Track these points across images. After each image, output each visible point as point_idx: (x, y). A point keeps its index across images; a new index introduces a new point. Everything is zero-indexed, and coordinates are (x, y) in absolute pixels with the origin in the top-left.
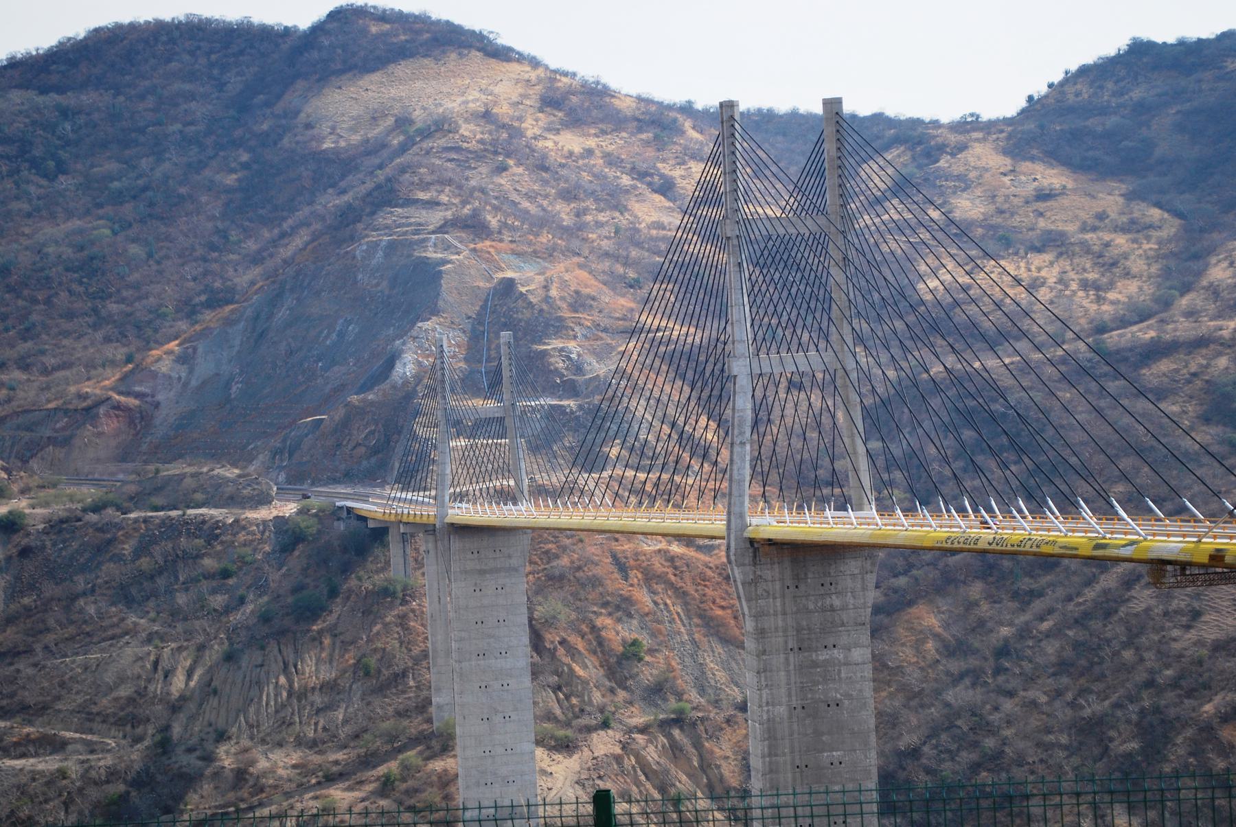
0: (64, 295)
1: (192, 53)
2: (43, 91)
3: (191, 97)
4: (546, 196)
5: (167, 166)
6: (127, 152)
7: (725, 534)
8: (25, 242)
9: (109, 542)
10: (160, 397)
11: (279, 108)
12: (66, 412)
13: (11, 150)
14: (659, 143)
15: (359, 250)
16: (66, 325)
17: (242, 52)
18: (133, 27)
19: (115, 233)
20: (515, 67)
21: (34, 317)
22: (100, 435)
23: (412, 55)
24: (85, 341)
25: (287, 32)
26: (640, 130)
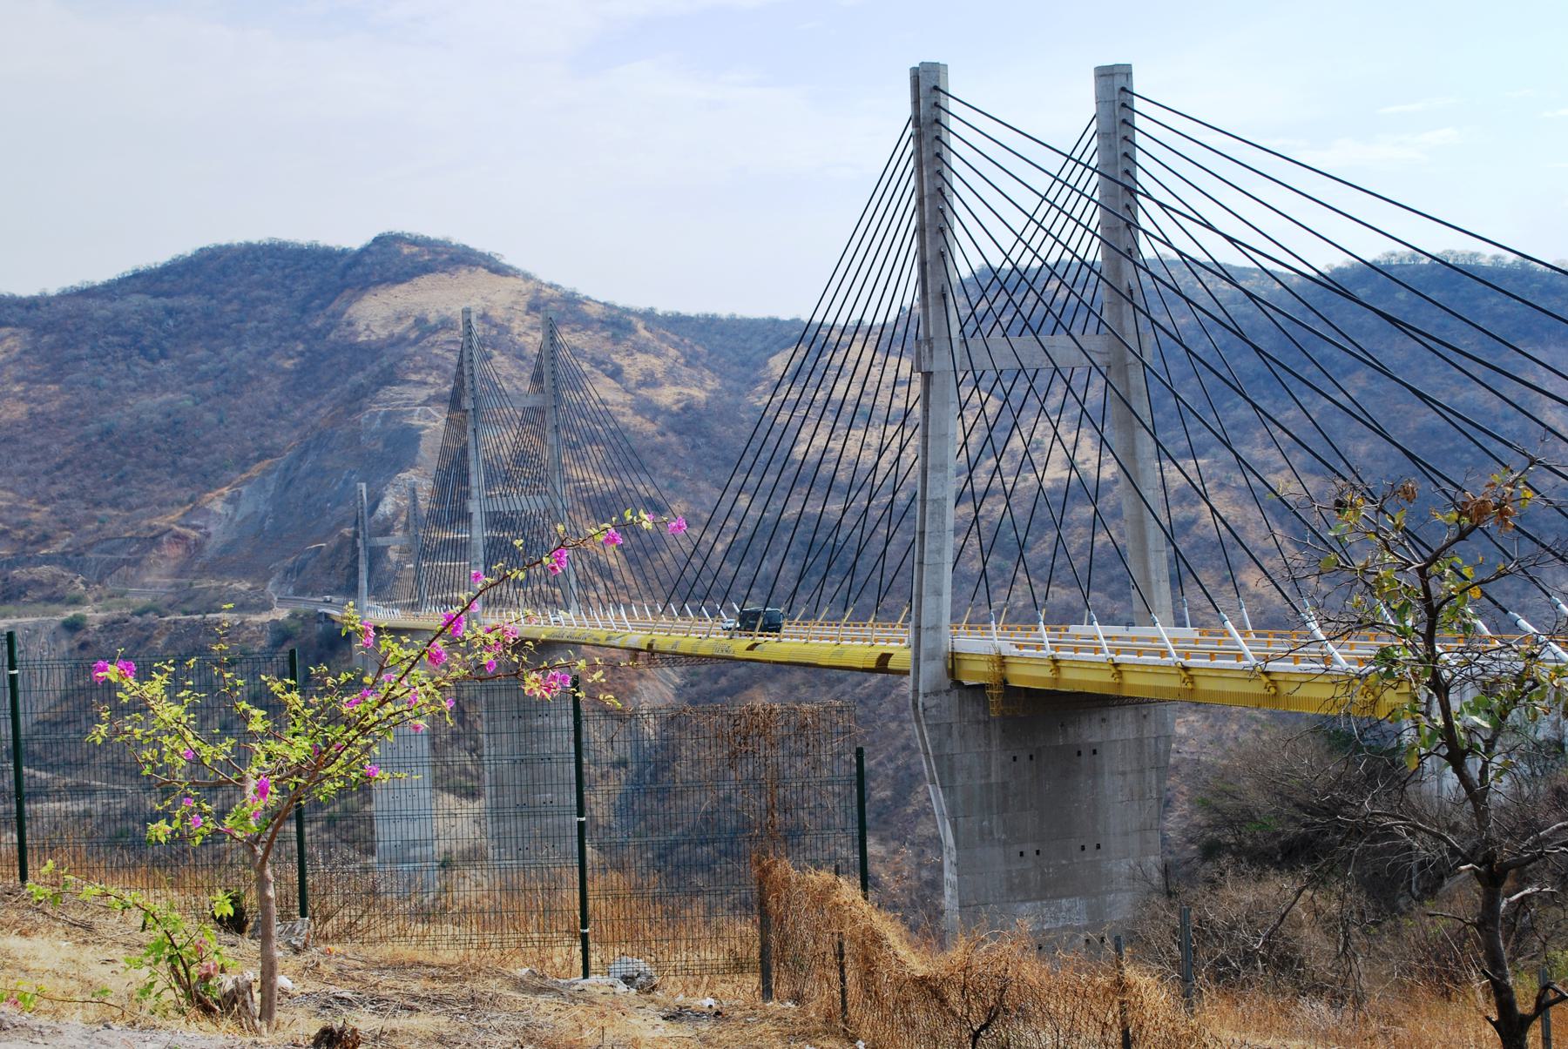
0: (152, 451)
1: (270, 268)
2: (156, 296)
3: (267, 301)
4: (520, 379)
5: (242, 353)
6: (216, 342)
7: (910, 667)
8: (127, 410)
9: (148, 638)
10: (211, 529)
11: (329, 311)
12: (138, 540)
13: (127, 340)
14: (615, 339)
15: (363, 418)
16: (149, 473)
17: (308, 268)
18: (229, 248)
19: (196, 404)
20: (511, 280)
21: (127, 468)
22: (163, 557)
23: (432, 271)
24: (164, 486)
25: (344, 252)
26: (603, 329)
